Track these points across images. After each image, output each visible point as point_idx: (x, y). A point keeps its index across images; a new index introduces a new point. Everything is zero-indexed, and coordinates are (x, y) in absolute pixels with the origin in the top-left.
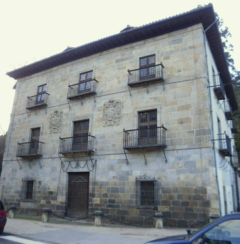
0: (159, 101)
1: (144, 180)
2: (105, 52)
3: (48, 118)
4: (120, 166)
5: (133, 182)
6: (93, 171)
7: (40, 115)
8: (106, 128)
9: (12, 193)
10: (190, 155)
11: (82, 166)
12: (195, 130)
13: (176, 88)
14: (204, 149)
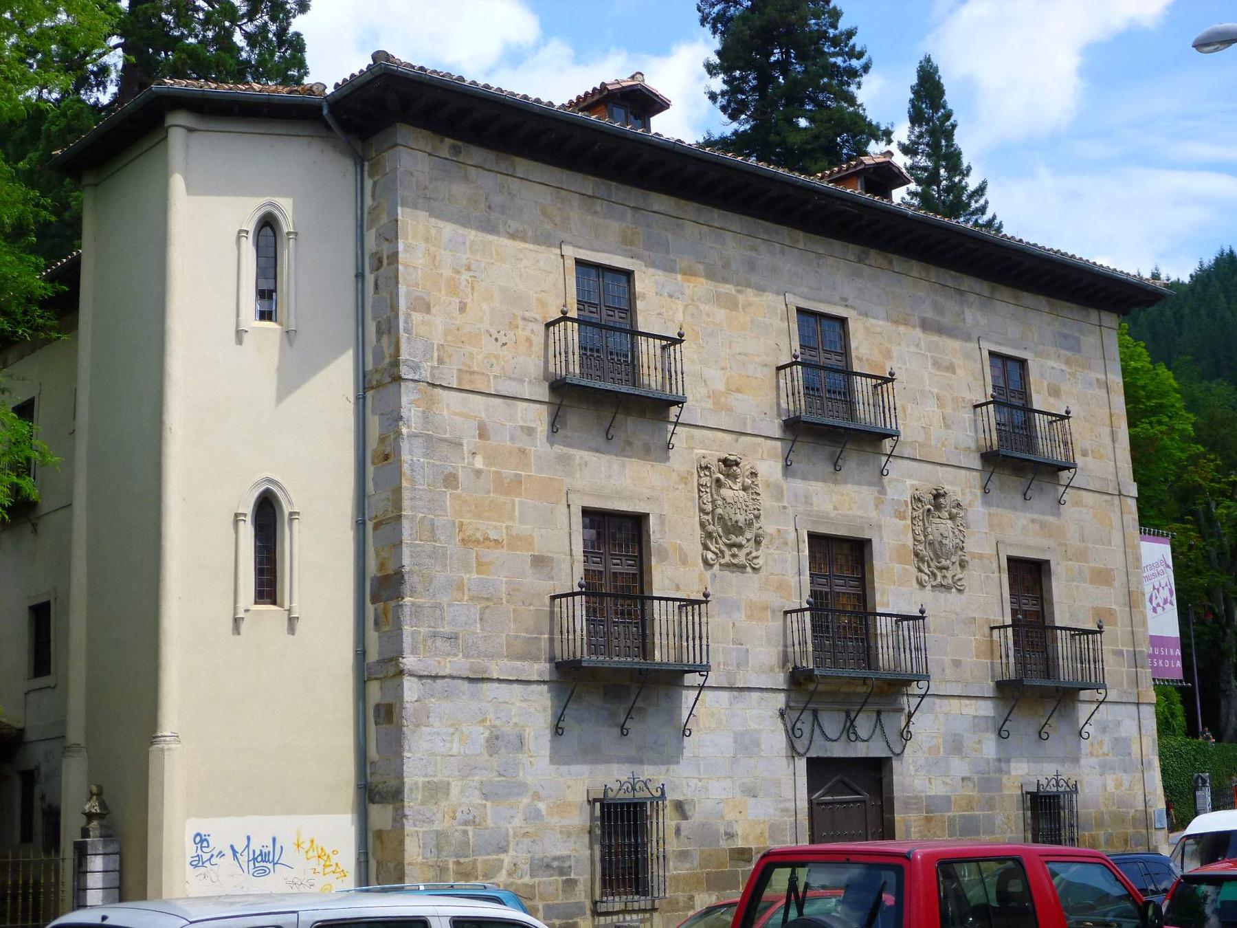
3: (684, 479)
5: (1012, 795)
9: (510, 874)
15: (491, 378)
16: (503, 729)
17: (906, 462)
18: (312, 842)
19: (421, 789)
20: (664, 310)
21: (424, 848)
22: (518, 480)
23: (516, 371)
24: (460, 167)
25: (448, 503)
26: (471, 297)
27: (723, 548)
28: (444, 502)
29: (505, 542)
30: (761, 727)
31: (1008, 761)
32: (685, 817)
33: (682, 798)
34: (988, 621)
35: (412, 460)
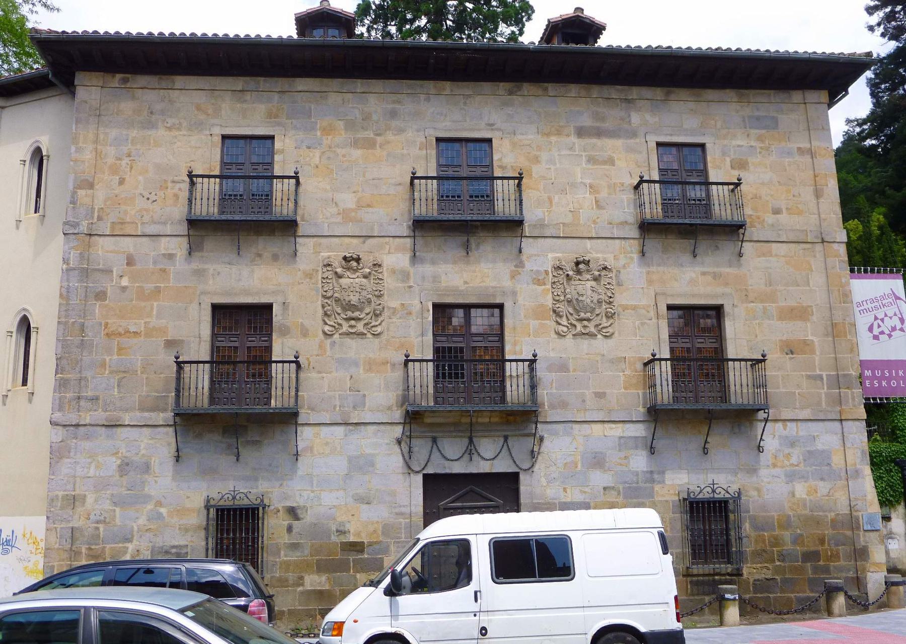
0: (727, 284)
1: (712, 495)
2: (552, 88)
5: (667, 501)
8: (569, 341)
10: (817, 436)
12: (824, 374)
13: (771, 256)
14: (850, 423)
15: (139, 224)
16: (133, 458)
17: (548, 240)
18: (31, 533)
19: (60, 500)
20: (302, 158)
21: (61, 538)
22: (158, 290)
23: (162, 217)
24: (128, 91)
25: (97, 311)
26: (129, 173)
27: (574, 322)
28: (94, 310)
29: (143, 333)
30: (377, 452)
31: (662, 473)
32: (297, 518)
33: (294, 505)
34: (640, 359)
35: (68, 285)
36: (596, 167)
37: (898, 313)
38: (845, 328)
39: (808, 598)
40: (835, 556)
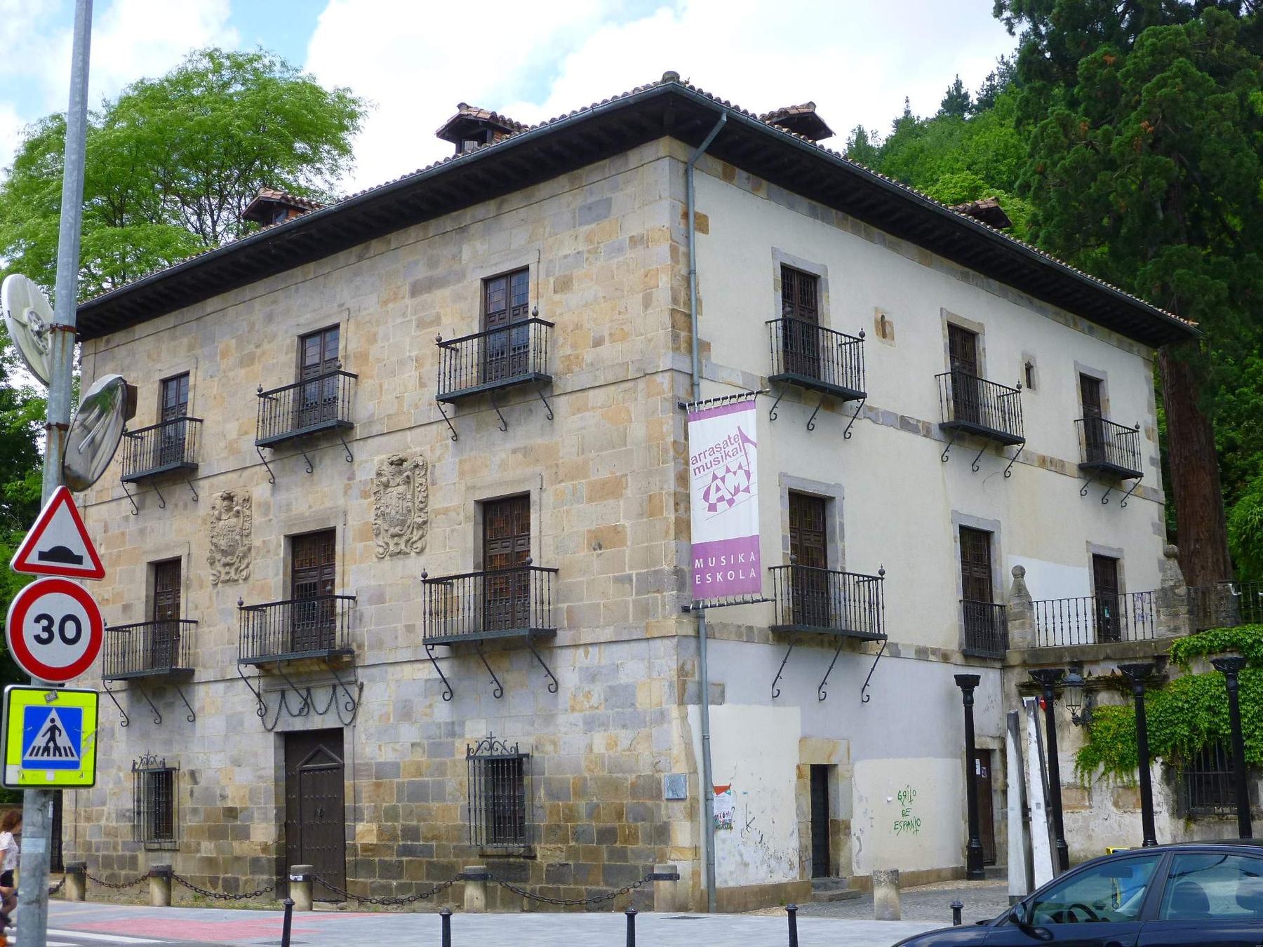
2: (376, 246)
3: (204, 521)
4: (431, 706)
6: (353, 724)
7: (176, 505)
11: (321, 709)
13: (587, 410)
32: (196, 782)
36: (425, 331)
37: (744, 464)
38: (661, 501)
39: (600, 892)
40: (633, 837)
